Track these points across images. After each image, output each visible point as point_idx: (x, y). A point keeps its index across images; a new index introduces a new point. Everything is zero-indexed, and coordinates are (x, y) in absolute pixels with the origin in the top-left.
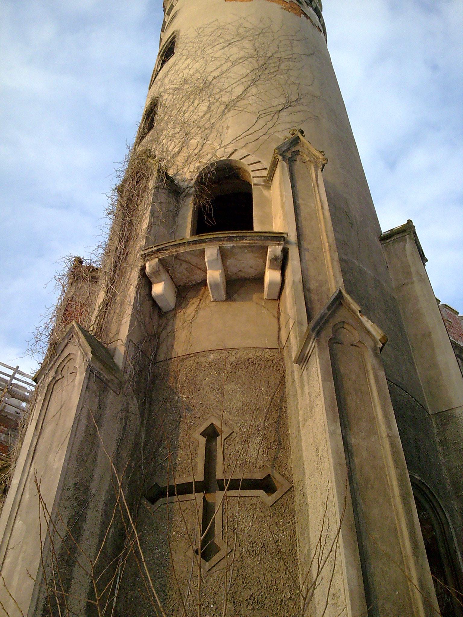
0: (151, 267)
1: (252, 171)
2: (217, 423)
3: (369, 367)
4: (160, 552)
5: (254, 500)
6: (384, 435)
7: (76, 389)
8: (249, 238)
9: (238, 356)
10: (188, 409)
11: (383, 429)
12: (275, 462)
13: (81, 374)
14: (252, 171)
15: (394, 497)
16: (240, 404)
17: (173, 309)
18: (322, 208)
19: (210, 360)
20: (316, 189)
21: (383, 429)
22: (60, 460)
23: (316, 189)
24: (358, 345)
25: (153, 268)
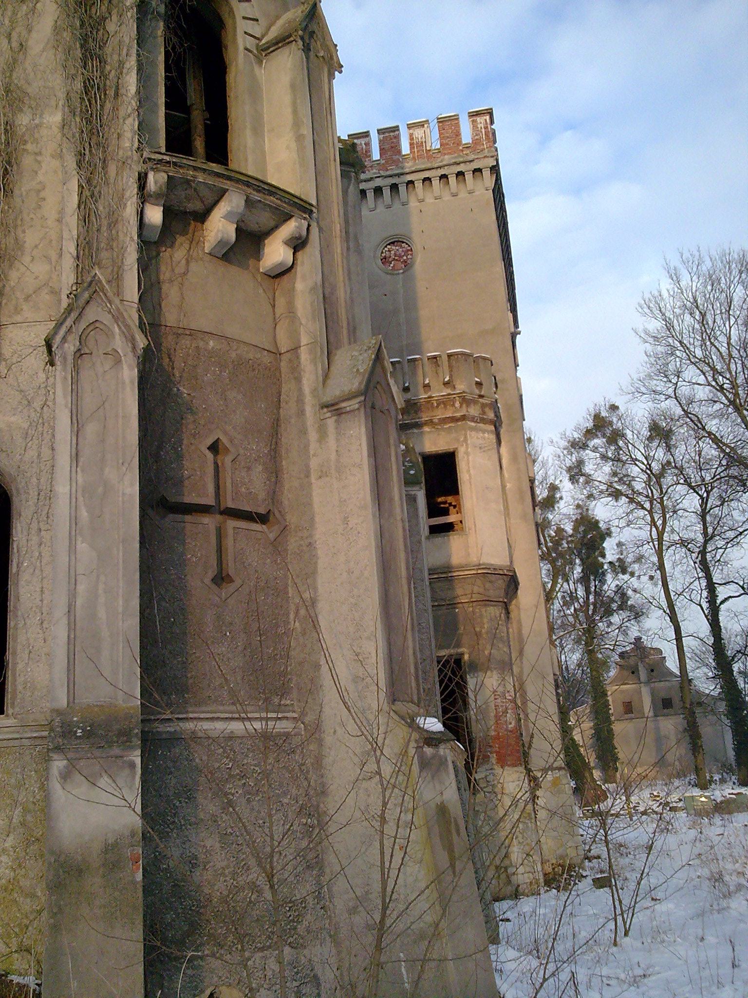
0: (158, 185)
1: (244, 18)
2: (224, 440)
3: (392, 442)
4: (175, 574)
5: (259, 536)
6: (399, 518)
7: (128, 389)
8: (279, 196)
9: (239, 352)
10: (193, 413)
11: (398, 510)
12: (274, 495)
13: (130, 366)
14: (244, 18)
15: (401, 577)
16: (243, 420)
17: (155, 243)
18: (335, 160)
19: (210, 347)
20: (329, 117)
21: (398, 510)
22: (132, 485)
23: (329, 117)
24: (386, 412)
25: (161, 188)
